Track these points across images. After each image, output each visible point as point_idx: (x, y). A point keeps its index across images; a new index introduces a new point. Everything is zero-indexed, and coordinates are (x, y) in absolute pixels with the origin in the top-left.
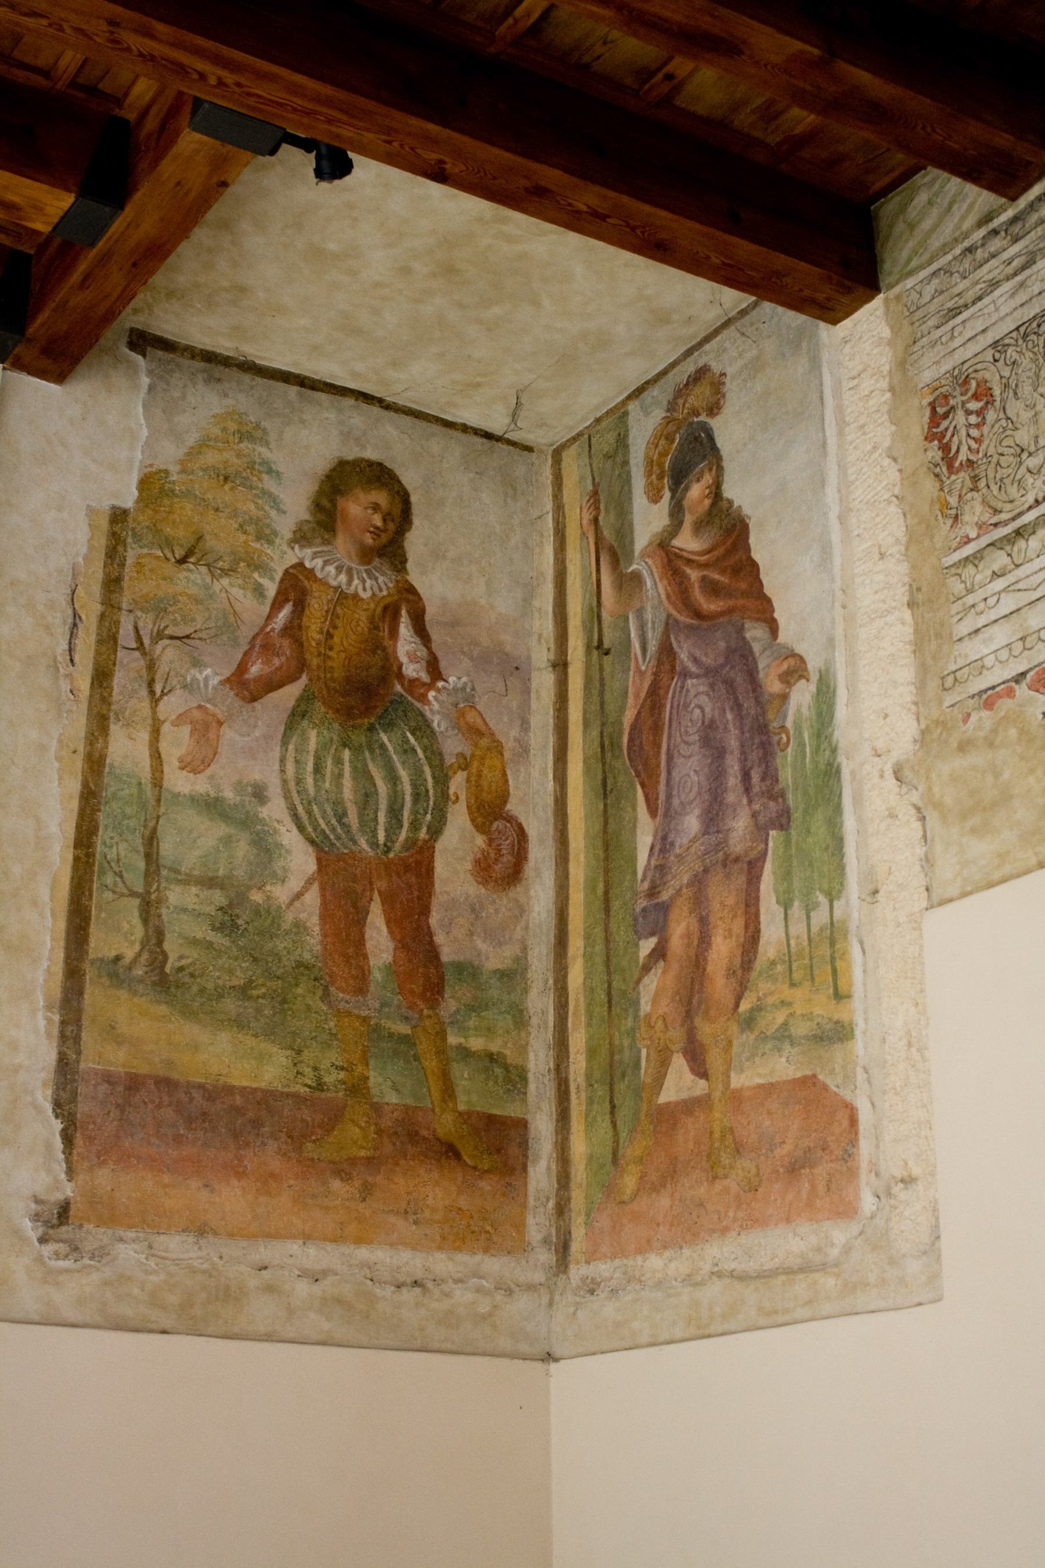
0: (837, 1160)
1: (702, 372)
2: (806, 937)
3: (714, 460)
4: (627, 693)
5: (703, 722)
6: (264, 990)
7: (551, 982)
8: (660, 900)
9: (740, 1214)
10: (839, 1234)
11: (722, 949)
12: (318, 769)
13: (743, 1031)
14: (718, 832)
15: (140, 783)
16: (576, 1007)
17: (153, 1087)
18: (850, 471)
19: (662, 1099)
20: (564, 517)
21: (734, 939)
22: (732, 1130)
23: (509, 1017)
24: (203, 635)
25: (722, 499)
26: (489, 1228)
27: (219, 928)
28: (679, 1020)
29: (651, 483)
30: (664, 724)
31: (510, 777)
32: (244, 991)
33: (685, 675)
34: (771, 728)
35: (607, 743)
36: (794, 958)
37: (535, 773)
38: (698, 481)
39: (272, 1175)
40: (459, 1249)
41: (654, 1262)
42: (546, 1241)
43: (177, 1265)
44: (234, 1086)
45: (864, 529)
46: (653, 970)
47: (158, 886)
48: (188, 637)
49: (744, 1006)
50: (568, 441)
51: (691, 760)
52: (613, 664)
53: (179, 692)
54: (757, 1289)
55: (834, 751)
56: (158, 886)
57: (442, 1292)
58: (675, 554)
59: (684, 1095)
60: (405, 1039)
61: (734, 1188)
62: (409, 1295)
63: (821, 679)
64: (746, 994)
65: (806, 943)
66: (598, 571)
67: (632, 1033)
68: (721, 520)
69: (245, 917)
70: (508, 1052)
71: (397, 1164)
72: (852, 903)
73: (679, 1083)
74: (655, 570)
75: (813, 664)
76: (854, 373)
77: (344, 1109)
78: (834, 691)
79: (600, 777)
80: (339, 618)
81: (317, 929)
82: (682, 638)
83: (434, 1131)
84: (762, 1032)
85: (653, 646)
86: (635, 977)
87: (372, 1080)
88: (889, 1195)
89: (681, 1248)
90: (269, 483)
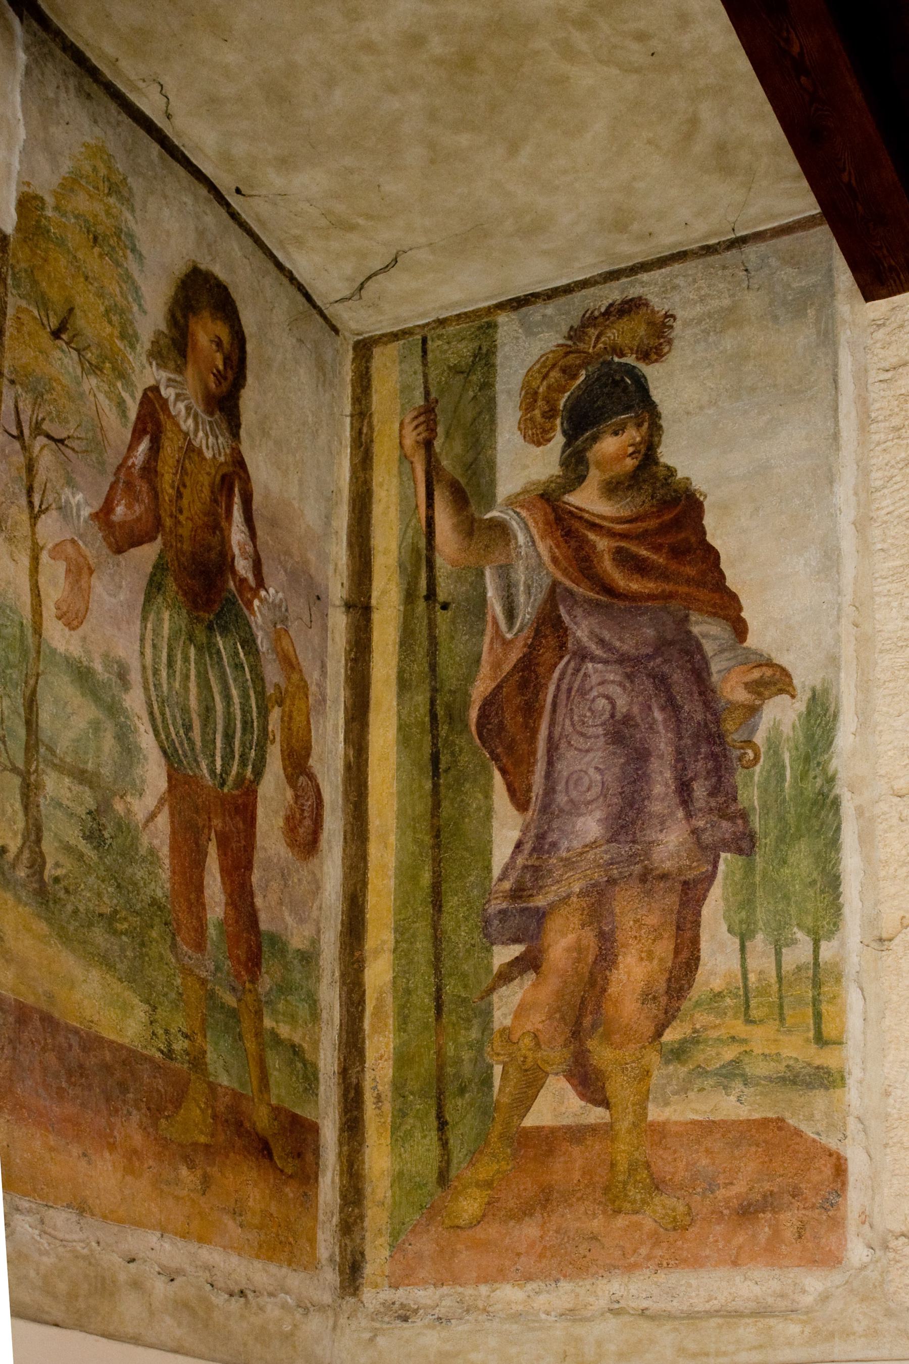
0: (813, 1207)
1: (630, 307)
2: (774, 973)
3: (647, 416)
4: (478, 661)
5: (612, 716)
6: (126, 926)
7: (337, 974)
8: (531, 905)
9: (659, 1252)
10: (813, 1283)
11: (635, 972)
12: (170, 664)
13: (668, 1062)
14: (634, 842)
15: (22, 624)
16: (378, 1009)
17: (38, 1023)
18: (874, 475)
19: (529, 1121)
20: (371, 427)
21: (656, 962)
22: (648, 1166)
23: (306, 1006)
24: (75, 444)
25: (657, 463)
26: (291, 1239)
27: (89, 837)
28: (561, 1040)
29: (531, 419)
30: (543, 707)
31: (312, 727)
32: (110, 920)
33: (583, 655)
34: (729, 739)
35: (441, 712)
36: (752, 994)
37: (330, 726)
38: (616, 433)
39: (135, 1152)
40: (270, 1259)
41: (510, 1294)
42: (331, 1260)
43: (65, 1246)
44: (103, 1038)
45: (892, 544)
46: (517, 981)
47: (37, 766)
48: (61, 441)
49: (671, 1036)
50: (383, 335)
51: (591, 755)
52: (453, 622)
53: (54, 513)
54: (676, 1330)
55: (831, 780)
56: (37, 766)
57: (258, 1305)
58: (570, 512)
59: (566, 1121)
60: (234, 1014)
61: (649, 1224)
62: (236, 1304)
63: (814, 698)
64: (674, 1024)
65: (774, 980)
66: (430, 505)
67: (478, 1047)
68: (654, 489)
69: (110, 830)
70: (305, 1046)
71: (227, 1157)
72: (850, 945)
73: (557, 1105)
74: (531, 523)
75: (804, 677)
76: (887, 365)
77: (188, 1083)
78: (835, 716)
79: (427, 750)
80: (187, 474)
81: (167, 861)
82: (579, 612)
83: (254, 1124)
84: (699, 1066)
85: (526, 612)
86: (484, 986)
87: (209, 1055)
88: (886, 1248)
89: (557, 1281)
90: (132, 265)
